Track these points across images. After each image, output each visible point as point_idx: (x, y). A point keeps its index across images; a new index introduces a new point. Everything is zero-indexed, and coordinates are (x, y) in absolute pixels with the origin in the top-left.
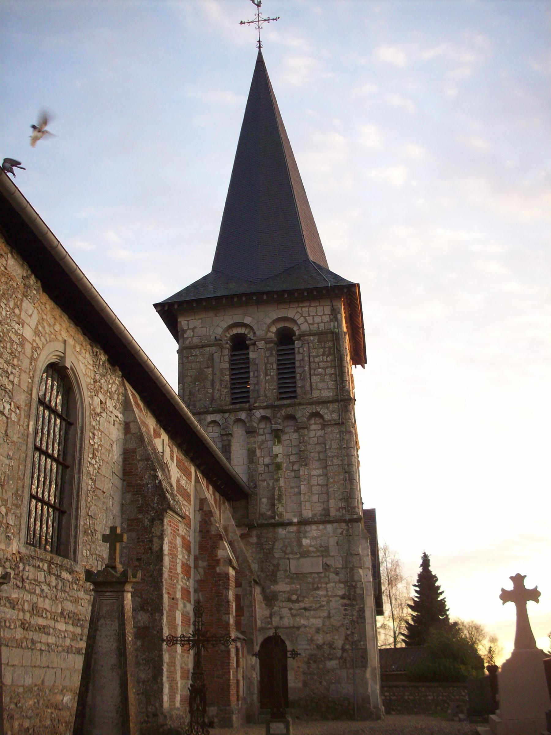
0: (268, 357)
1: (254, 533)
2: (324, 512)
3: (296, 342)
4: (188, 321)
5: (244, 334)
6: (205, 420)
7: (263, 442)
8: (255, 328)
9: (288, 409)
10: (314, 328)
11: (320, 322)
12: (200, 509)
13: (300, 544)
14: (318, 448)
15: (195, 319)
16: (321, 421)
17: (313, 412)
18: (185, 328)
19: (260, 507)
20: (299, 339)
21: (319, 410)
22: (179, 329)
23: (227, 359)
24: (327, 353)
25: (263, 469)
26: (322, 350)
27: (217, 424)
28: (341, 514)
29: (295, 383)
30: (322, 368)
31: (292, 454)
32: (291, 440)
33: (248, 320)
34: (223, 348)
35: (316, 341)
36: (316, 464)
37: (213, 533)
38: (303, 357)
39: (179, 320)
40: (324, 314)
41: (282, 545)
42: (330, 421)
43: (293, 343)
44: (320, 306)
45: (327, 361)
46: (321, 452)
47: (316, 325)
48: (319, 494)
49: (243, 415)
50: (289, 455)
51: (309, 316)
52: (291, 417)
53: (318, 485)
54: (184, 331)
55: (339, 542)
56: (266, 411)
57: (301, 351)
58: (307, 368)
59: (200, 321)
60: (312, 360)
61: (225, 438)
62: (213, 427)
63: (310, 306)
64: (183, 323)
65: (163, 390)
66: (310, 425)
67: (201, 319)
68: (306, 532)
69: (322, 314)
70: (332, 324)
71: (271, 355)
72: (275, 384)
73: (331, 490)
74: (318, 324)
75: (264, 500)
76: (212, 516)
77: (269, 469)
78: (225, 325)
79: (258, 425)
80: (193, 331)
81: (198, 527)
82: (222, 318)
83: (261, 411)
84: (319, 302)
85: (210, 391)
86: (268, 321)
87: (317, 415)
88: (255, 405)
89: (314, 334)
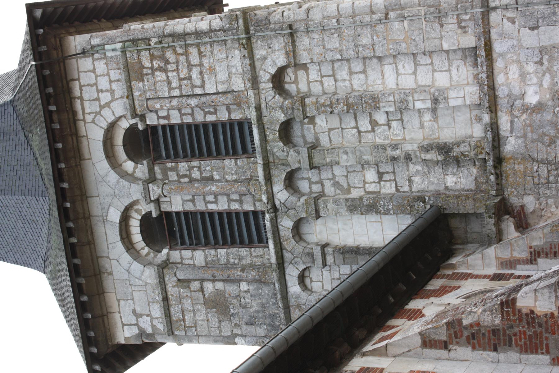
0: (178, 175)
1: (514, 201)
2: (469, 60)
3: (148, 123)
4: (123, 325)
5: (141, 221)
6: (298, 297)
7: (336, 184)
8: (127, 202)
9: (270, 137)
10: (120, 89)
11: (106, 78)
12: (446, 347)
13: (539, 107)
14: (343, 74)
15: (119, 312)
16: (290, 71)
17: (274, 87)
18: (135, 331)
19: (463, 190)
20: (143, 118)
21: (268, 77)
22: (139, 342)
23: (187, 254)
24: (162, 64)
25: (388, 184)
26: (157, 73)
27: (307, 274)
28: (471, 24)
29: (224, 124)
30: (190, 70)
31: (357, 127)
32: (330, 130)
33: (115, 216)
34: (168, 259)
35: (141, 84)
36: (374, 76)
37: (498, 321)
38: (172, 108)
39: (123, 342)
40: (94, 71)
41: (540, 145)
42: (287, 54)
43: (154, 128)
44: (78, 79)
45: (177, 63)
46: (350, 68)
47: (114, 86)
48: (434, 71)
49: (286, 224)
50: (359, 132)
51: (98, 99)
52: (286, 131)
53: (415, 73)
54: (142, 333)
55: (531, 24)
56: (275, 179)
57: (163, 113)
58: (193, 102)
59: (122, 303)
60: (176, 93)
61: (330, 259)
62: (312, 281)
63: (81, 98)
64: (127, 334)
65: (282, 349)
66: (299, 92)
67: (119, 301)
68: (510, 95)
69: (93, 75)
70: (109, 54)
71: (175, 169)
72: (227, 162)
73: (422, 47)
74: (111, 82)
75: (450, 181)
76: (460, 321)
77: (387, 173)
78: (126, 258)
79: (304, 195)
80: (141, 316)
81: (486, 354)
82: (114, 262)
83: (276, 189)
84: (74, 80)
85: (244, 286)
86: (113, 176)
87: (278, 80)
88: (265, 201)
89: (130, 89)
